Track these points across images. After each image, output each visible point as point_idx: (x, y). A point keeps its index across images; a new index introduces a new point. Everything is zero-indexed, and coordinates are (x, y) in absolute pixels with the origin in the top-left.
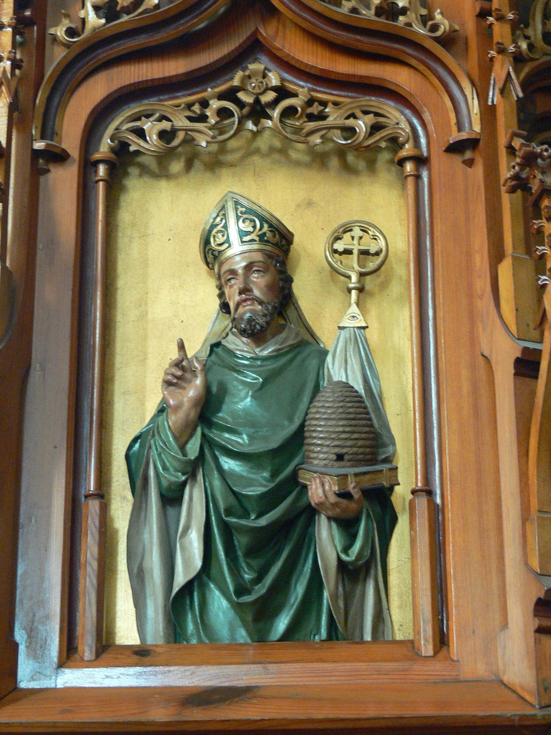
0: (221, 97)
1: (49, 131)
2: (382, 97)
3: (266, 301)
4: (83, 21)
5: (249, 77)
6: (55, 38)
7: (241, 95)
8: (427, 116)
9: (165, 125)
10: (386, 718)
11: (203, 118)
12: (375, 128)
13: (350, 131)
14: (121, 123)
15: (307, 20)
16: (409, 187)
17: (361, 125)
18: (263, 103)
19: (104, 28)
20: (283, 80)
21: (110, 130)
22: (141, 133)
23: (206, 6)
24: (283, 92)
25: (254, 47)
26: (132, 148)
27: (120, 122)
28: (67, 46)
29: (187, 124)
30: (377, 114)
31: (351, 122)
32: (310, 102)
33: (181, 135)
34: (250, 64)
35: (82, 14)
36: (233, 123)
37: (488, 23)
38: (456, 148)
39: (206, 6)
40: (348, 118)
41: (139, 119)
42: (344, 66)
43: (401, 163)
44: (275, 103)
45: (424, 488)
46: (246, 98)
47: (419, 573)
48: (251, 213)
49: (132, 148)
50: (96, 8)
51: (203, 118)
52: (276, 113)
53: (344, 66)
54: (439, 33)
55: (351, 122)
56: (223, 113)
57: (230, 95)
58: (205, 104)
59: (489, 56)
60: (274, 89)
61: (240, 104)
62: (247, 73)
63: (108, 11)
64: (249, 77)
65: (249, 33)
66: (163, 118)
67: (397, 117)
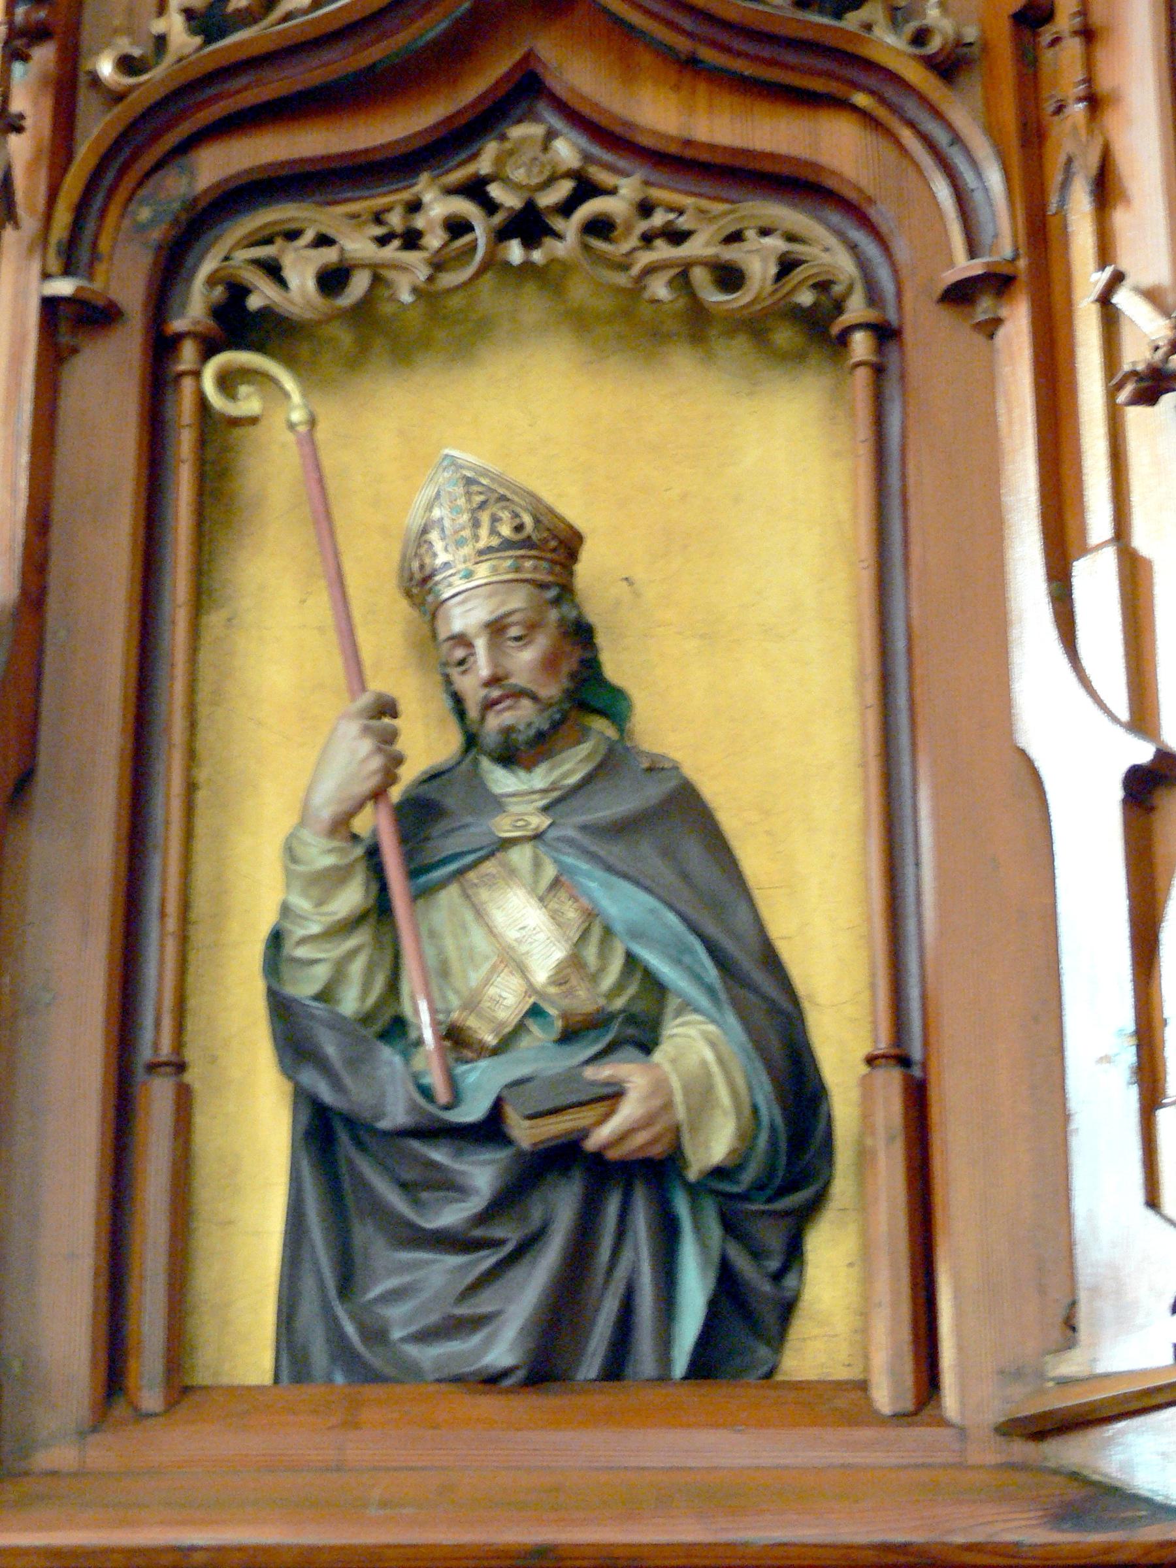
1: (84, 254)
3: (486, 763)
4: (161, 41)
5: (511, 153)
6: (95, 81)
7: (495, 191)
8: (902, 252)
9: (329, 255)
11: (412, 239)
12: (787, 265)
14: (232, 249)
15: (160, 977)
16: (930, 127)
17: (758, 261)
19: (197, 55)
20: (587, 158)
21: (207, 267)
22: (273, 270)
24: (586, 189)
25: (526, 90)
26: (254, 302)
27: (224, 253)
28: (117, 97)
30: (791, 238)
31: (731, 254)
32: (645, 209)
35: (158, 26)
36: (473, 247)
41: (269, 241)
42: (724, 126)
44: (567, 208)
45: (893, 1052)
47: (883, 1228)
48: (486, 495)
49: (254, 302)
50: (189, 14)
51: (412, 239)
52: (570, 227)
53: (724, 126)
54: (935, 44)
56: (457, 227)
58: (415, 207)
60: (570, 174)
61: (490, 207)
62: (508, 145)
63: (208, 23)
64: (511, 153)
65: (517, 56)
66: (323, 241)
67: (830, 252)
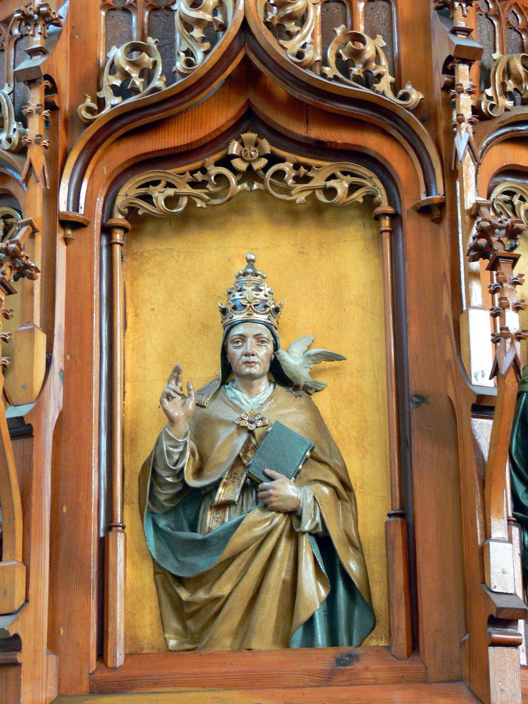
0: (217, 164)
2: (497, 627)
9: (171, 192)
10: (387, 550)
11: (202, 185)
13: (331, 192)
17: (341, 186)
18: (255, 169)
22: (148, 198)
23: (517, 424)
29: (188, 190)
31: (332, 183)
33: (184, 201)
34: (243, 133)
37: (451, 94)
38: (425, 210)
39: (517, 424)
40: (328, 179)
43: (378, 218)
44: (265, 169)
46: (238, 164)
55: (332, 183)
57: (226, 161)
59: (452, 123)
66: (170, 185)
